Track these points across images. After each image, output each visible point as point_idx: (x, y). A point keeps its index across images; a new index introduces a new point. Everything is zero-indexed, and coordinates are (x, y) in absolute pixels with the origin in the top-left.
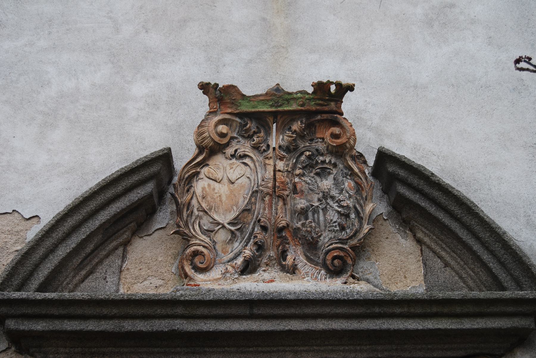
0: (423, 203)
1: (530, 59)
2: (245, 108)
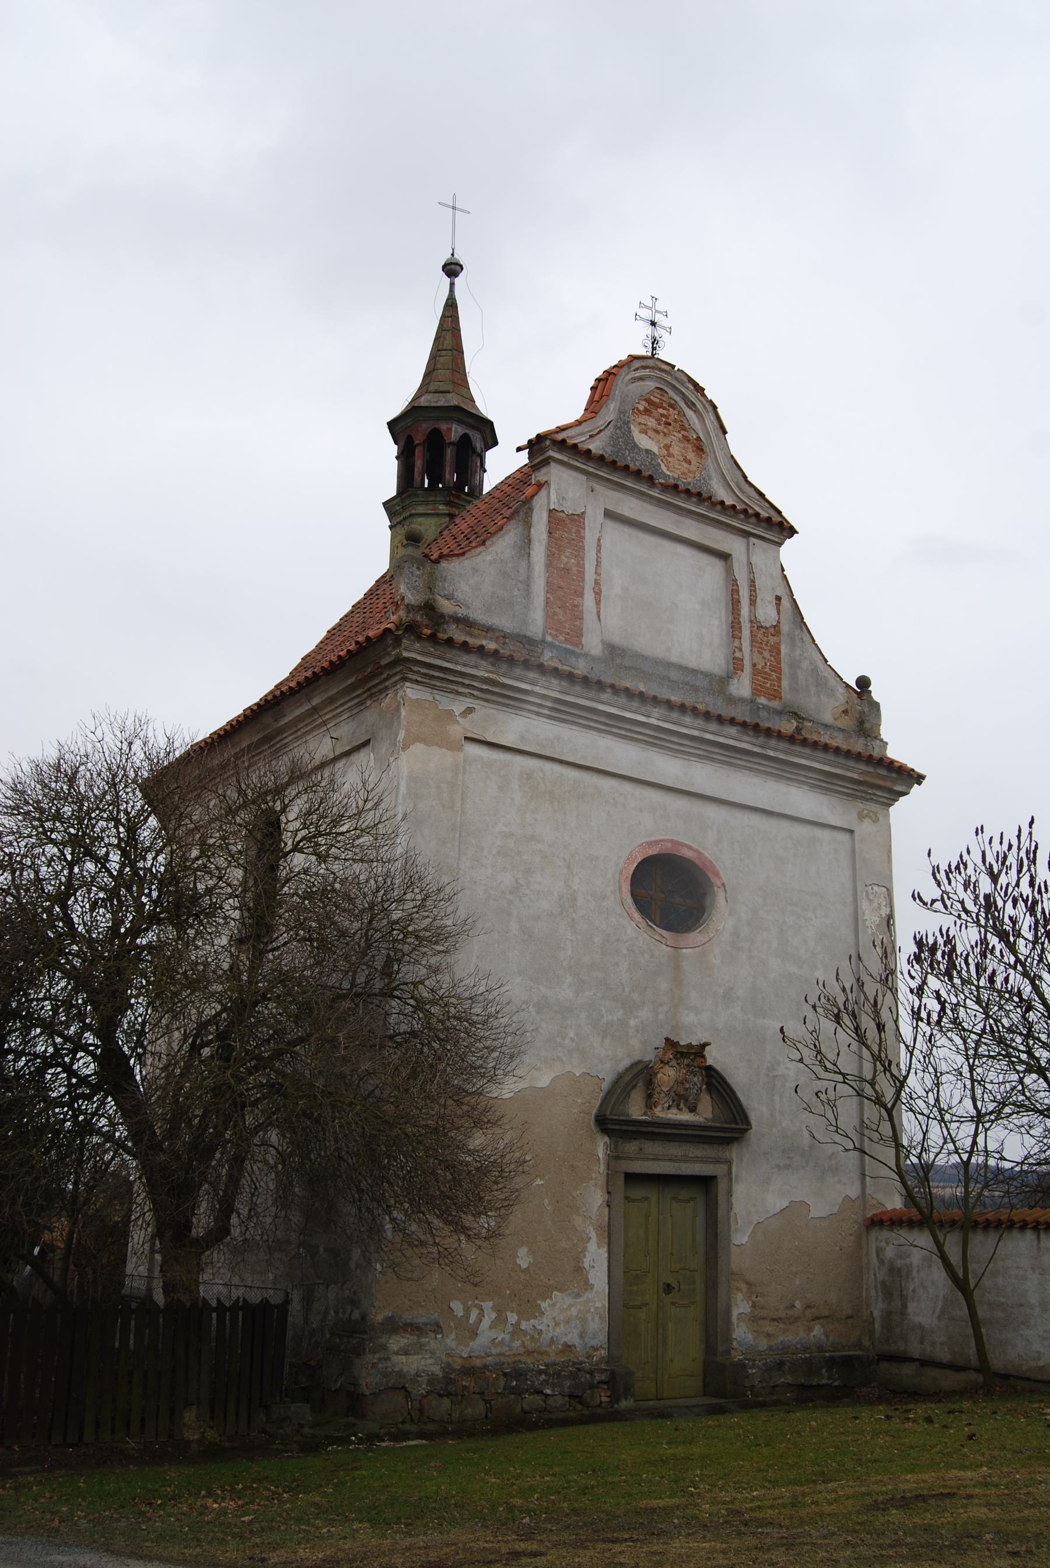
0: (719, 1087)
1: (922, 1366)
2: (679, 1049)
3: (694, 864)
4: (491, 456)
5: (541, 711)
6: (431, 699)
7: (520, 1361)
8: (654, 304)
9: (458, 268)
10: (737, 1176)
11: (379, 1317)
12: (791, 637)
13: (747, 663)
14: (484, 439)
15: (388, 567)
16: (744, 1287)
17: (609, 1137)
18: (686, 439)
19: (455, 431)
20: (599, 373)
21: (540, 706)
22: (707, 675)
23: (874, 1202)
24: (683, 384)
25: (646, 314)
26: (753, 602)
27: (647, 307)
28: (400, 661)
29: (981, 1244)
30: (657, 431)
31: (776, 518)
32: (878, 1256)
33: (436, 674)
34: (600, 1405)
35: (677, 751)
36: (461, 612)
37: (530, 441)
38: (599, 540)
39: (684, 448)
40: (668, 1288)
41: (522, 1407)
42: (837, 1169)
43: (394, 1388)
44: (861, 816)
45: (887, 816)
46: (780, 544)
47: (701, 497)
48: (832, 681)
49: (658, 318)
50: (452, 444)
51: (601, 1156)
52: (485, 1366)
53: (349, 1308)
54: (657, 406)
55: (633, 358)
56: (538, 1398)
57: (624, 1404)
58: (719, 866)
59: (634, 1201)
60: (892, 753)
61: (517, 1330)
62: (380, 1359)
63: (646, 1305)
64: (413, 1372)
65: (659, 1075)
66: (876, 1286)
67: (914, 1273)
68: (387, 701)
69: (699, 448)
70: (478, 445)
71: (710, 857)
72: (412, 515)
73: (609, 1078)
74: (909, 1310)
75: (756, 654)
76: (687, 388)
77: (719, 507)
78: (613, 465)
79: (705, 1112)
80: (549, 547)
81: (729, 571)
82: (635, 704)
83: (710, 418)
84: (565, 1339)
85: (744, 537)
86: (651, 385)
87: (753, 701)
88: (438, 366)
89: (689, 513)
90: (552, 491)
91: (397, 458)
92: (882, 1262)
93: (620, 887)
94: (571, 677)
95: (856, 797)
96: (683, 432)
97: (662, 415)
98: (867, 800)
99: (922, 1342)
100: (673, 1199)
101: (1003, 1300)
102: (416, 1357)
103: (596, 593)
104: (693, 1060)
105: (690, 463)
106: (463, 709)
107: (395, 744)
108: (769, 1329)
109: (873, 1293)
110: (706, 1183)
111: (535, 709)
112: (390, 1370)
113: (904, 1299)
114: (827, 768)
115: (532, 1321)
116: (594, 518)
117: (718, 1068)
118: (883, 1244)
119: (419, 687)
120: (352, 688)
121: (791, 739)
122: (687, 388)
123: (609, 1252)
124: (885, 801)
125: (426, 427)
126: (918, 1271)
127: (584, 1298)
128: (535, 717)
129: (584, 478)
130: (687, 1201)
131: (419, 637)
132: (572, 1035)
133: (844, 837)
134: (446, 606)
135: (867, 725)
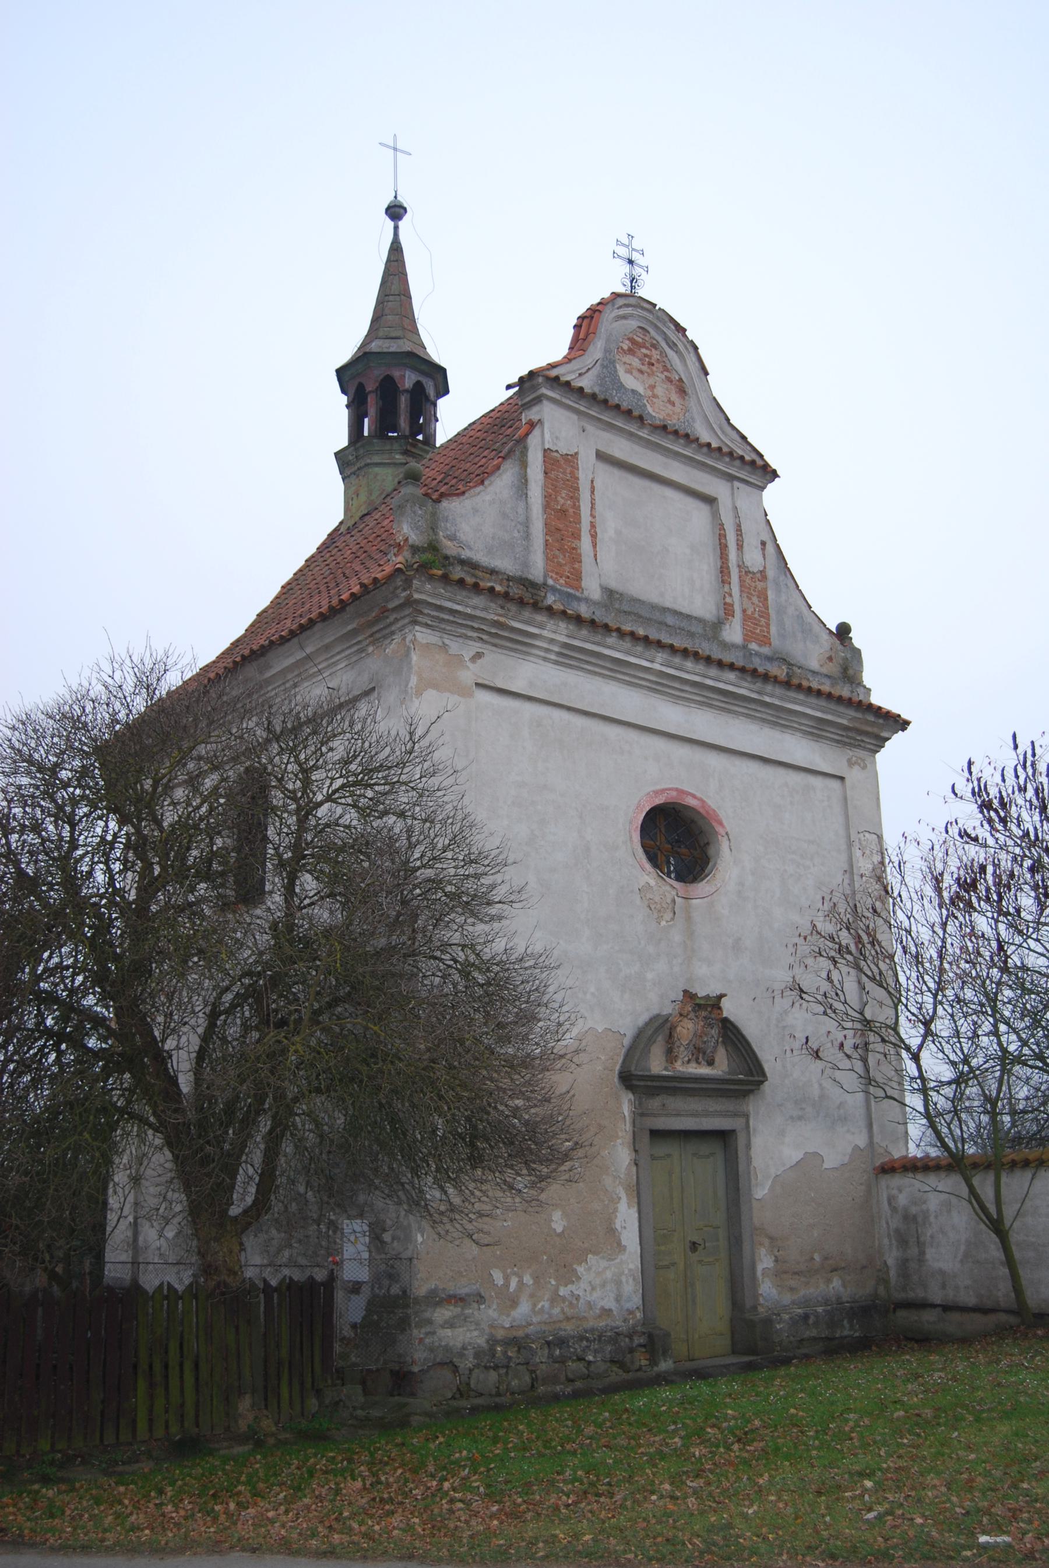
2: (698, 1001)
3: (698, 813)
4: (443, 405)
5: (548, 656)
6: (440, 644)
7: (560, 1329)
8: (630, 242)
9: (402, 211)
10: (754, 1130)
11: (421, 1288)
12: (777, 584)
13: (737, 608)
14: (436, 387)
15: (341, 517)
16: (766, 1241)
17: (633, 1094)
18: (669, 380)
19: (409, 379)
20: (582, 310)
21: (547, 650)
22: (700, 620)
23: (882, 1151)
24: (664, 324)
25: (623, 252)
26: (740, 547)
27: (623, 245)
28: (409, 602)
29: (1014, 1184)
30: (641, 372)
31: (760, 462)
32: (890, 1204)
33: (446, 617)
34: (639, 1369)
35: (678, 697)
36: (465, 554)
37: (521, 379)
38: (592, 482)
39: (667, 389)
40: (694, 1246)
41: (566, 1376)
42: (845, 1118)
43: (442, 1364)
44: (851, 763)
45: (874, 762)
46: (763, 488)
47: (689, 439)
48: (817, 627)
49: (635, 256)
50: (407, 391)
51: (626, 1114)
52: (527, 1336)
53: (386, 1282)
54: (642, 346)
55: (616, 295)
56: (581, 1365)
57: (665, 1365)
58: (722, 815)
59: (660, 1158)
60: (876, 700)
61: (555, 1298)
62: (427, 1334)
63: (674, 1264)
64: (459, 1345)
65: (679, 1029)
66: (889, 1235)
67: (932, 1219)
68: (392, 647)
69: (682, 391)
70: (431, 392)
71: (713, 806)
72: (367, 465)
73: (630, 1033)
74: (928, 1256)
75: (745, 599)
76: (669, 328)
77: (705, 450)
78: (605, 404)
79: (721, 1067)
80: (545, 487)
81: (716, 515)
82: (639, 649)
83: (691, 359)
84: (602, 1303)
85: (728, 481)
86: (633, 324)
87: (745, 647)
88: (387, 311)
89: (677, 455)
90: (546, 431)
91: (347, 406)
92: (894, 1209)
93: (631, 837)
94: (578, 620)
95: (845, 744)
96: (666, 373)
97: (646, 356)
98: (855, 746)
99: (944, 1286)
100: (694, 1154)
101: (1033, 1240)
102: (461, 1330)
103: (592, 536)
104: (710, 1012)
105: (673, 404)
106: (472, 653)
107: (406, 692)
108: (793, 1283)
109: (886, 1241)
110: (724, 1137)
111: (542, 654)
112: (437, 1344)
113: (921, 1245)
114: (819, 714)
115: (570, 1286)
116: (587, 462)
117: (732, 1019)
118: (895, 1192)
119: (429, 631)
120: (355, 632)
121: (787, 684)
122: (669, 328)
123: (639, 1212)
124: (872, 747)
125: (378, 373)
126: (936, 1217)
127: (618, 1261)
128: (541, 662)
129: (575, 417)
130: (708, 1157)
131: (431, 578)
132: (592, 990)
133: (835, 784)
134: (450, 548)
135: (851, 672)
